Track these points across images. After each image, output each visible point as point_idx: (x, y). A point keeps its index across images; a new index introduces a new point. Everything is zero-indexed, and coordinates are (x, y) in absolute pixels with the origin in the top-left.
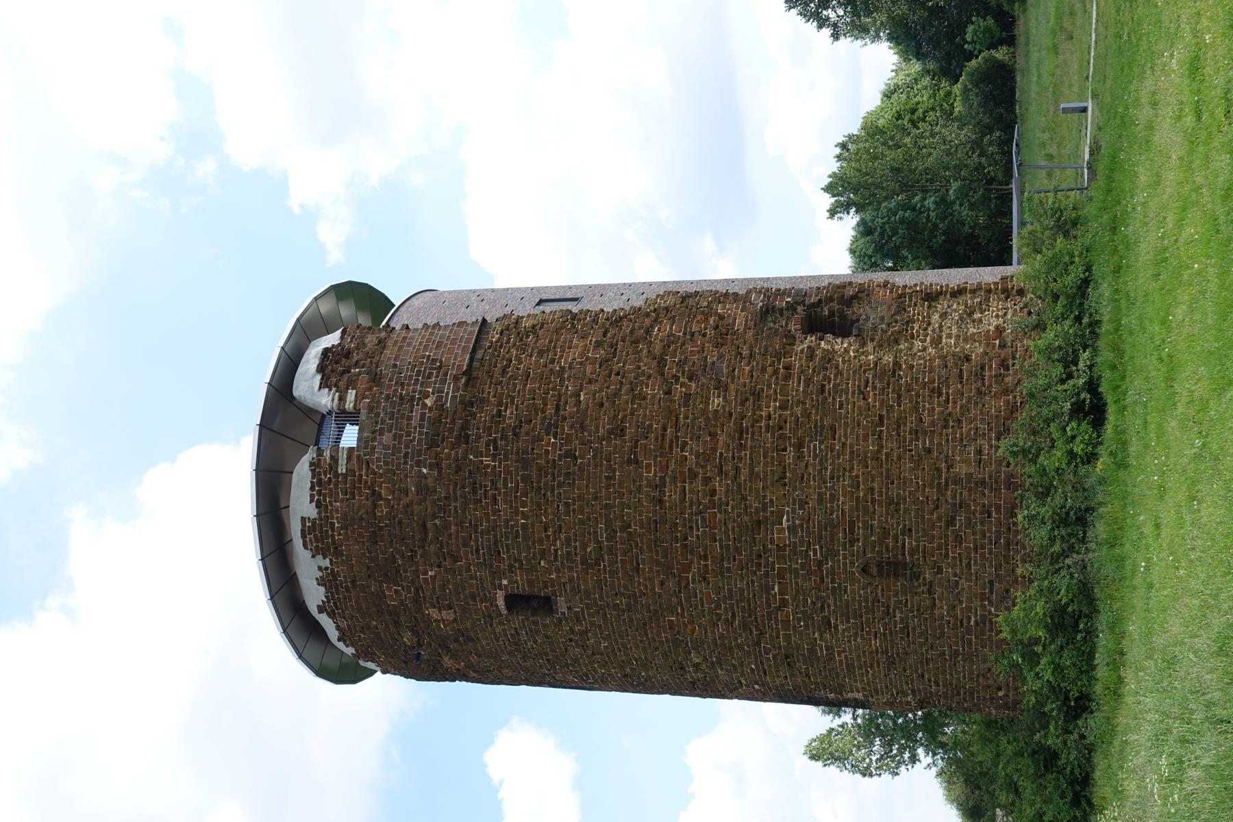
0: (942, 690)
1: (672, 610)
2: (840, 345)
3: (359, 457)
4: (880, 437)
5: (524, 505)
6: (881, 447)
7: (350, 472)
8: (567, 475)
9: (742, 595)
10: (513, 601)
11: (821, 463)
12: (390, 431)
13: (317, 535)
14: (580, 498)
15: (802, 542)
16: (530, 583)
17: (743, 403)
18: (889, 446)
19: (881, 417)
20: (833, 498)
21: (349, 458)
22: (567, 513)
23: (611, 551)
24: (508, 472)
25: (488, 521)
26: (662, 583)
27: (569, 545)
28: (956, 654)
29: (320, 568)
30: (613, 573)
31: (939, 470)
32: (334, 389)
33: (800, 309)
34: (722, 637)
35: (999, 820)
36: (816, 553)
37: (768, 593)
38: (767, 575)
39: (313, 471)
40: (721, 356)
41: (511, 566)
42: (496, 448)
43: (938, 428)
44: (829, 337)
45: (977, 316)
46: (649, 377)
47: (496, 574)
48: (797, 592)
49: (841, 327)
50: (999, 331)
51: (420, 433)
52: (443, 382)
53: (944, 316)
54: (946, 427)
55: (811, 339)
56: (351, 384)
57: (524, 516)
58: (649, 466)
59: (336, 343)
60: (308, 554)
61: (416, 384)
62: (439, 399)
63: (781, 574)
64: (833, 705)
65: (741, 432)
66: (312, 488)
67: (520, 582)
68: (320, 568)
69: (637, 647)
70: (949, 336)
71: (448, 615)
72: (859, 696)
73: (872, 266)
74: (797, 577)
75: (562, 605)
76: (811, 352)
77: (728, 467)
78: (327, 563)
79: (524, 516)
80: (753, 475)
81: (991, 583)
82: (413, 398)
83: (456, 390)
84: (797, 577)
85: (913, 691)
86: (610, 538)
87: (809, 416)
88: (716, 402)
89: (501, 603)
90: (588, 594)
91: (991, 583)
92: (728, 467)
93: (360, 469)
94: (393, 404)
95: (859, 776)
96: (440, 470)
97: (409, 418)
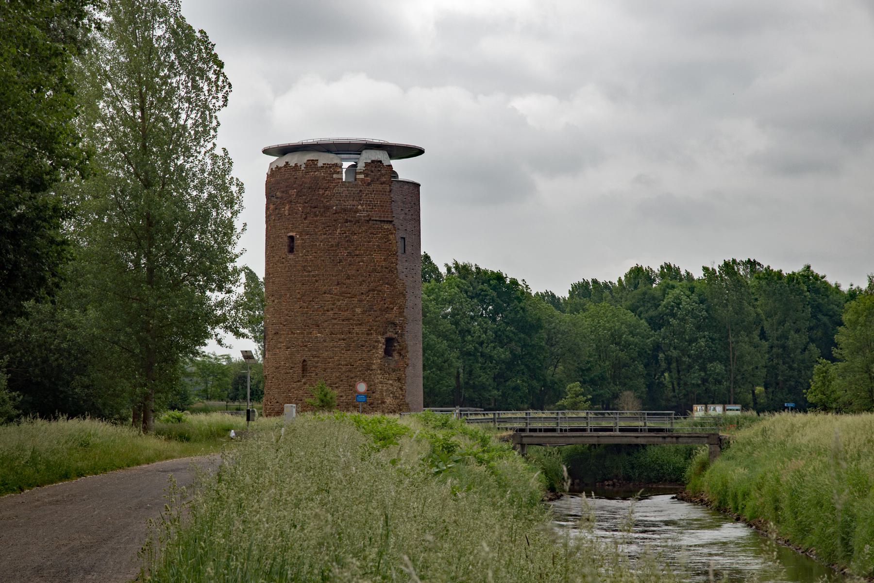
0: (269, 384)
1: (291, 296)
2: (381, 352)
3: (339, 182)
4: (347, 365)
5: (324, 245)
6: (343, 366)
7: (334, 179)
8: (333, 260)
9: (296, 320)
10: (292, 238)
11: (338, 347)
12: (349, 193)
13: (311, 164)
14: (326, 265)
15: (312, 340)
16: (298, 246)
17: (358, 320)
18: (344, 369)
19: (353, 365)
20: (327, 351)
21: (339, 179)
22: (321, 260)
23: (309, 276)
24: (334, 238)
25: (318, 231)
26: (299, 293)
27: (310, 261)
28: (281, 389)
29: (301, 166)
30: (302, 276)
31: (336, 384)
32: (364, 169)
33: (396, 336)
34: (283, 312)
35: (0, 418)
36: (310, 345)
37: (297, 329)
38: (302, 329)
39: (334, 164)
40: (375, 311)
41: (303, 239)
42: (343, 234)
43: (349, 384)
44: (384, 347)
45: (391, 395)
46: (368, 286)
47: (301, 234)
48: (297, 339)
49: (388, 352)
50: (383, 402)
51: (348, 205)
52: (367, 211)
53: (392, 385)
54: (350, 386)
55: (383, 341)
56: (367, 175)
57: (320, 245)
58: (336, 289)
59: (384, 164)
60: (305, 161)
61: (366, 201)
62: (361, 211)
63: (302, 333)
64: (264, 354)
65: (348, 320)
66: (328, 164)
67: (298, 242)
68: (301, 166)
69: (279, 281)
70: (382, 386)
71: (287, 213)
72: (267, 356)
73: (741, 286)
74: (302, 338)
75: (291, 256)
76: (378, 342)
77: (336, 316)
78: (303, 169)
79: (320, 245)
80: (334, 324)
81: (301, 400)
82: (360, 200)
83: (364, 216)
84: (302, 338)
85: (268, 375)
86: (313, 276)
87: (353, 342)
88: (358, 310)
89: (291, 234)
90: (295, 266)
91: (301, 400)
92: (336, 316)
93: (335, 183)
94: (359, 193)
95: (244, 186)
96: (335, 214)
97: (353, 200)
